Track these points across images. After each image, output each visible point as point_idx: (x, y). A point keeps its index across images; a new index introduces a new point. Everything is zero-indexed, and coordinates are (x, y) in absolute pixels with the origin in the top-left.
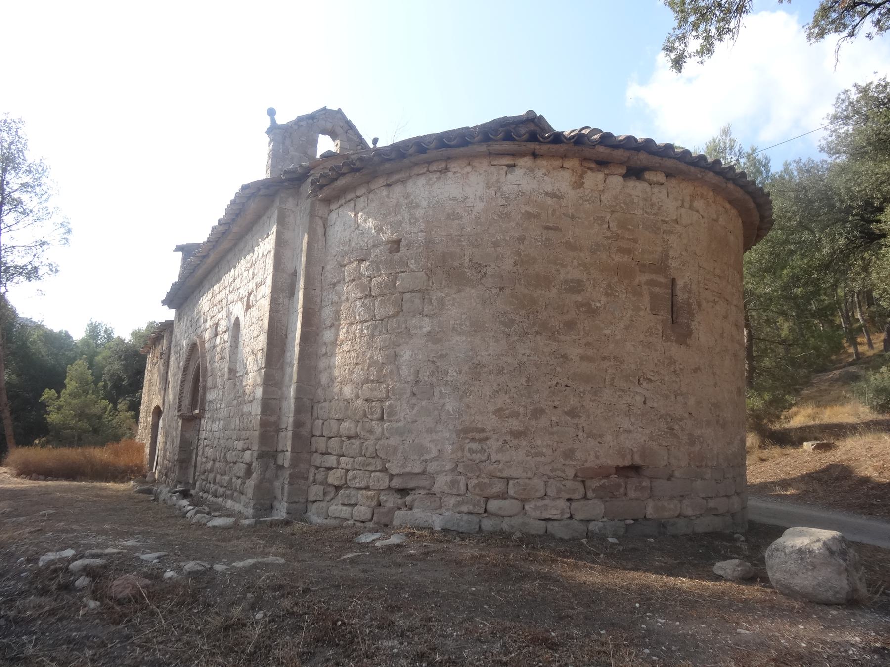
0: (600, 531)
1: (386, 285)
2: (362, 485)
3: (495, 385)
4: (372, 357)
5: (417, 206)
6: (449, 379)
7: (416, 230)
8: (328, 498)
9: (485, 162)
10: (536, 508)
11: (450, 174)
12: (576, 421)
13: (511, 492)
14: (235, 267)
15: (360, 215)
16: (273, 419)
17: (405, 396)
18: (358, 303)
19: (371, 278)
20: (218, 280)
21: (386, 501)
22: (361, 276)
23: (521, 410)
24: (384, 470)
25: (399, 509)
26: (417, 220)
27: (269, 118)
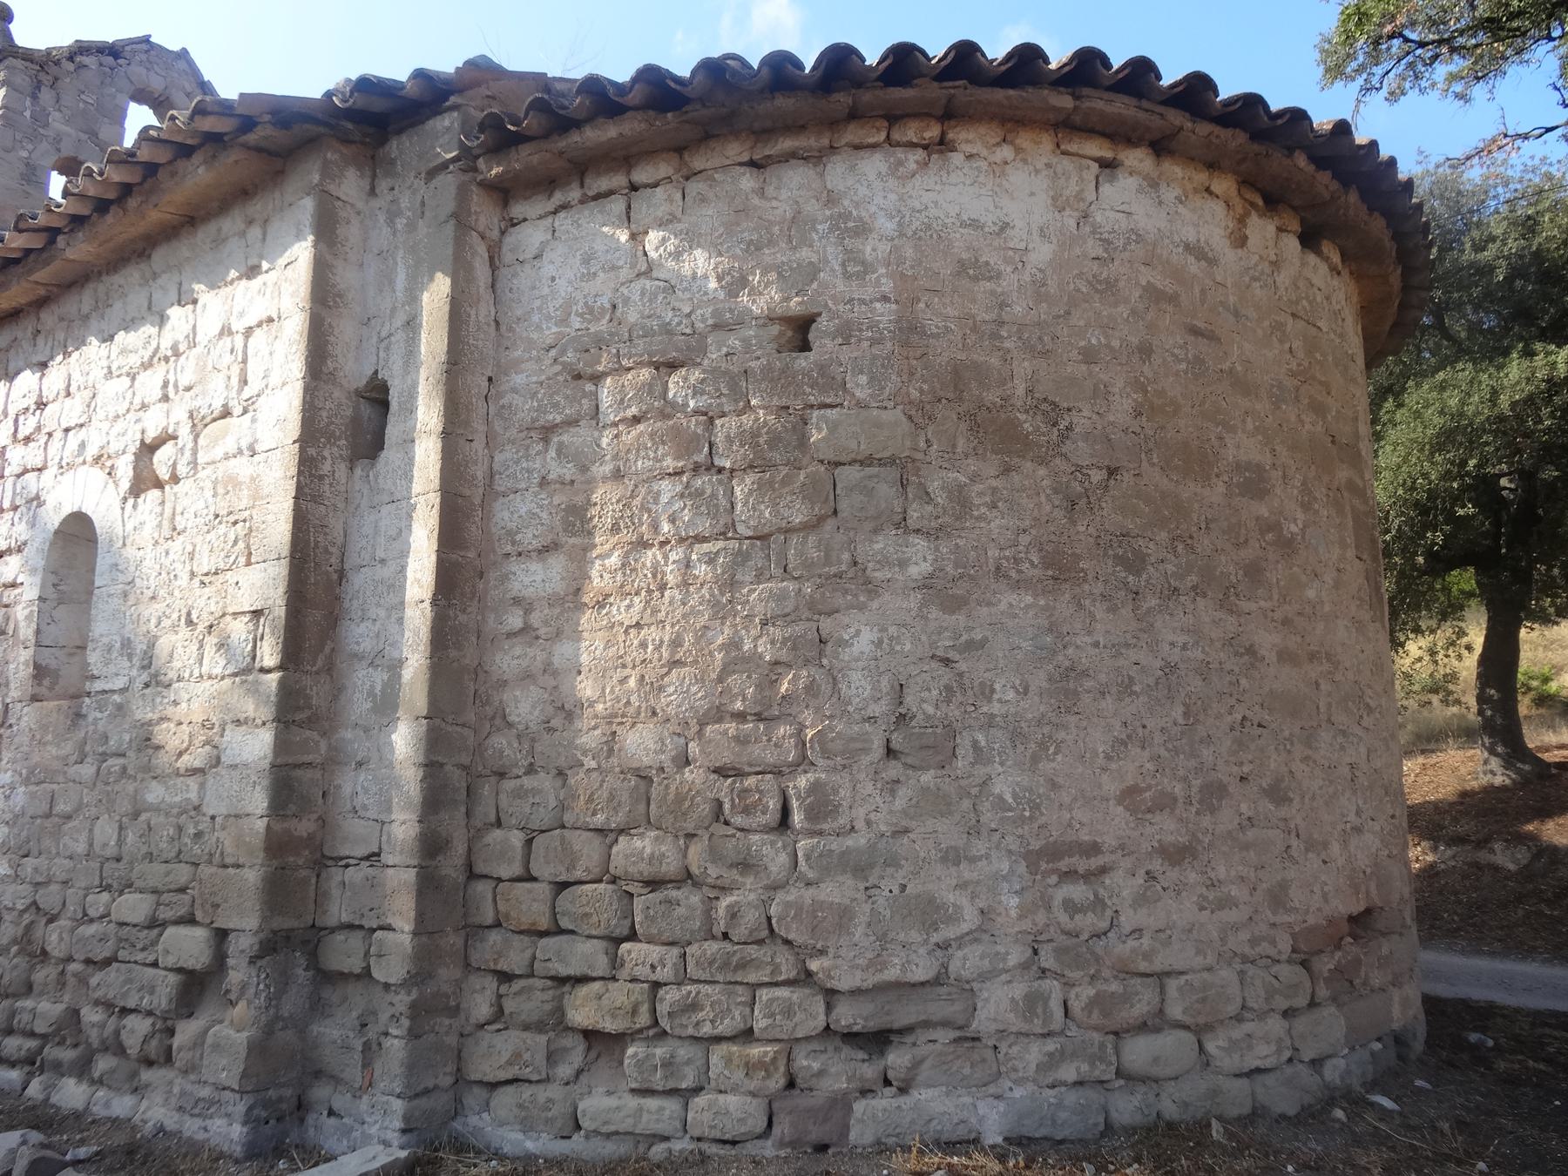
0: (1342, 1078)
1: (775, 440)
2: (725, 1027)
3: (1118, 725)
4: (733, 644)
5: (863, 230)
6: (996, 708)
7: (868, 292)
8: (564, 1070)
9: (1047, 141)
10: (1233, 1046)
11: (957, 158)
12: (1283, 812)
13: (1175, 1011)
15: (654, 237)
16: (304, 827)
17: (866, 760)
18: (667, 488)
19: (709, 418)
21: (821, 1073)
22: (668, 410)
23: (1178, 789)
24: (805, 978)
25: (865, 1092)
26: (868, 269)
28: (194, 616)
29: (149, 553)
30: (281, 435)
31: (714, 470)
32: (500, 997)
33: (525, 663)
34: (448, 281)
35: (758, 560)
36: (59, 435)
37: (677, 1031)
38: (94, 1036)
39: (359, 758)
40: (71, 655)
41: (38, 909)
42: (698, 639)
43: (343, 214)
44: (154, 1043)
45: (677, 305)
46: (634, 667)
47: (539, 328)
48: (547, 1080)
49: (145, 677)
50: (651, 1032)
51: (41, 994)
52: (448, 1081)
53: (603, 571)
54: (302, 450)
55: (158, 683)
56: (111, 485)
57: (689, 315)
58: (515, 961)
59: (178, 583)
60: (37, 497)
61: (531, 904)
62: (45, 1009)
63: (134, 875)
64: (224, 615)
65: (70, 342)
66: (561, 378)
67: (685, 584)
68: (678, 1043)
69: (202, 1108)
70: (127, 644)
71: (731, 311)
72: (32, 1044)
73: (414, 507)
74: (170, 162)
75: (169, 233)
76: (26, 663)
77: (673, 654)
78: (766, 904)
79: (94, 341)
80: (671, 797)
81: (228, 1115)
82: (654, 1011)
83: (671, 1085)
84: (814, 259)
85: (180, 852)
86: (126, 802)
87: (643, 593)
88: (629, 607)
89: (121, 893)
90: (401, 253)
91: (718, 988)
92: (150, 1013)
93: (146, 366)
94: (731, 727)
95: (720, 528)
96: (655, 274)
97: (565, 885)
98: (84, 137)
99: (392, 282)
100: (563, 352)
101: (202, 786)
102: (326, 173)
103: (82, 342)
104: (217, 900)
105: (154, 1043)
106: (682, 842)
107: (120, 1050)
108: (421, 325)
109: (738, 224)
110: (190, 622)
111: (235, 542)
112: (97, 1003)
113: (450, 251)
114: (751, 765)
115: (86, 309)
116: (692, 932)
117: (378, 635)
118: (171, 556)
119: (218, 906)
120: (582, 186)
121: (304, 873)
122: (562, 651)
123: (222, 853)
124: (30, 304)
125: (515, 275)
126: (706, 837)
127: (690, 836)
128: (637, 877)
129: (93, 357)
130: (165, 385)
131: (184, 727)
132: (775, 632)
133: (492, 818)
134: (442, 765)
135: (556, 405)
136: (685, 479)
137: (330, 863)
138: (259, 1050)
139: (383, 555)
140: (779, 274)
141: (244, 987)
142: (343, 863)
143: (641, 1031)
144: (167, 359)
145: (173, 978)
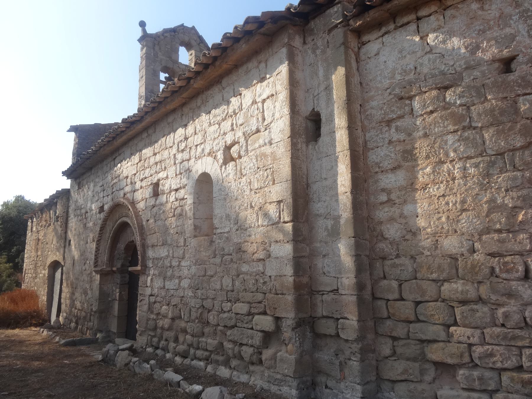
4: (492, 200)
8: (428, 378)
14: (185, 126)
16: (305, 280)
18: (451, 139)
19: (467, 107)
20: (151, 143)
22: (447, 106)
27: (140, 29)
28: (253, 205)
29: (233, 184)
30: (282, 136)
31: (471, 129)
32: (394, 346)
33: (390, 214)
34: (344, 69)
35: (500, 164)
36: (194, 148)
37: (484, 365)
38: (230, 353)
39: (324, 254)
40: (204, 221)
41: (204, 307)
42: (474, 200)
43: (296, 52)
44: (255, 357)
45: (447, 62)
46: (444, 213)
47: (380, 82)
48: (421, 381)
49: (236, 227)
50: (470, 365)
51: (208, 336)
52: (374, 378)
54: (292, 140)
55: (241, 229)
56: (216, 162)
57: (453, 65)
58: (400, 331)
59: (246, 193)
60: (189, 169)
61: (406, 309)
62: (212, 342)
63: (240, 297)
64: (266, 203)
65: (195, 115)
66: (394, 100)
67: (465, 177)
68: (484, 370)
69: (279, 383)
70: (228, 217)
71: (473, 60)
72: (207, 353)
73: (338, 157)
74: (231, 46)
75: (228, 72)
76: (191, 225)
77: (462, 206)
78: (522, 312)
79: (204, 115)
80: (469, 266)
81: (289, 386)
82: (471, 356)
83: (483, 388)
84: (513, 31)
85: (258, 289)
86: (234, 271)
87: (445, 182)
88: (438, 189)
89: (235, 303)
90: (320, 63)
91: (502, 348)
92: (252, 346)
93: (224, 120)
94: (496, 236)
95: (479, 152)
96: (434, 51)
97: (420, 302)
98: (168, 59)
99: (317, 74)
100: (394, 89)
101: (264, 265)
102: (290, 38)
103: (199, 116)
104: (276, 306)
105: (255, 357)
106: (476, 285)
107: (241, 358)
108: (333, 88)
109: (472, 24)
110: (252, 207)
111: (267, 177)
112: (230, 341)
113: (343, 57)
114: (507, 252)
115: (199, 104)
116: (486, 323)
117: (327, 207)
118: (242, 184)
119: (276, 309)
120: (395, 23)
121: (306, 297)
122: (408, 209)
123: (276, 290)
124: (179, 106)
125: (367, 63)
126: (488, 283)
127: (480, 282)
128: (456, 299)
129: (204, 119)
130: (232, 125)
131: (254, 244)
132: (514, 194)
133: (382, 276)
134: (360, 255)
135: (393, 111)
136: (459, 133)
137: (315, 293)
138: (299, 362)
139: (325, 176)
140: (496, 41)
141: (290, 339)
142: (321, 293)
143: (465, 364)
144: (231, 116)
145: (260, 334)
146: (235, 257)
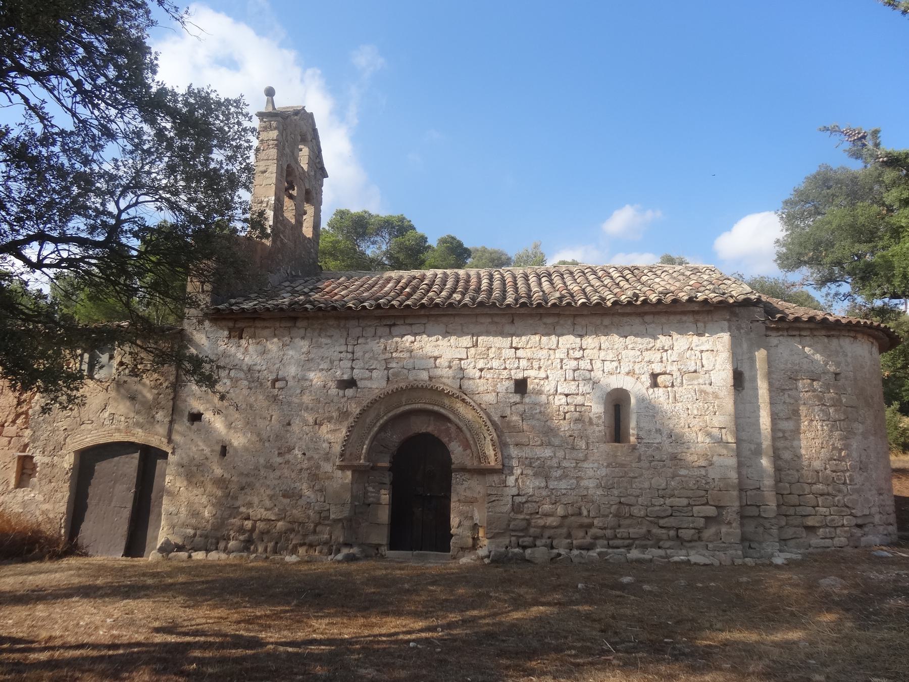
4: (833, 444)
22: (814, 391)
53: (805, 424)
122: (795, 443)
130: (662, 358)
146: (668, 463)
